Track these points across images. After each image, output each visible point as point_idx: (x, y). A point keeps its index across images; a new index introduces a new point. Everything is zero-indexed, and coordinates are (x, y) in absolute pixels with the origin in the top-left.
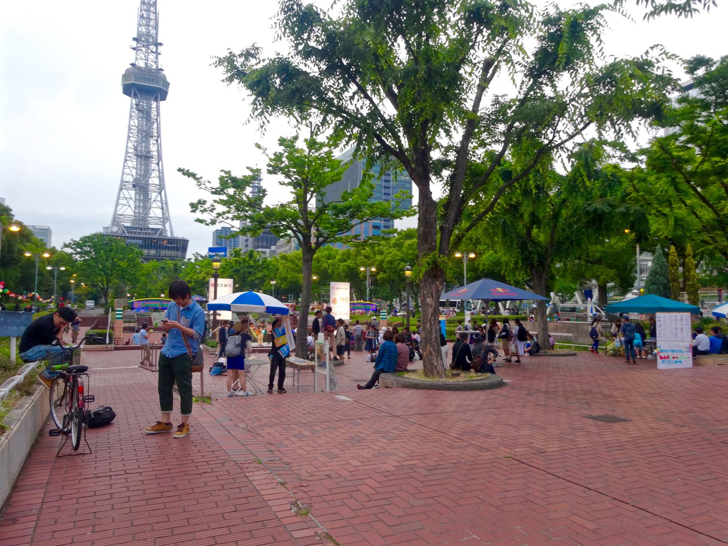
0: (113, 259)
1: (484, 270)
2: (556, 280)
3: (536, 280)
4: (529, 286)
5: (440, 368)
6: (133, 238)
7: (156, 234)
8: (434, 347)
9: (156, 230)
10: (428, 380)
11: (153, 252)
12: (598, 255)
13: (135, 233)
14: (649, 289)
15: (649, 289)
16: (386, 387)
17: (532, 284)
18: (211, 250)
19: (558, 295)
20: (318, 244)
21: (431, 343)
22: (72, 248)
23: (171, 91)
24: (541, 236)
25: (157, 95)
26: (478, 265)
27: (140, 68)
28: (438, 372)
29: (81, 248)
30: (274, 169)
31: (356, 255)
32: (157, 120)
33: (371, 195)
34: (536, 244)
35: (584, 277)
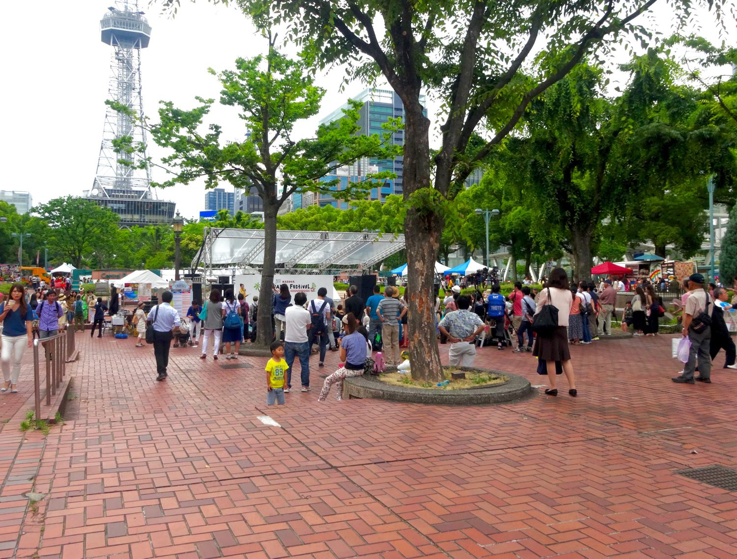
0: (84, 224)
1: (511, 230)
2: (600, 241)
3: (577, 239)
4: (567, 250)
5: (433, 366)
6: (116, 202)
7: (140, 197)
8: (426, 334)
9: (140, 193)
10: (418, 387)
11: (136, 217)
12: (655, 209)
13: (117, 196)
14: (727, 250)
15: (727, 250)
16: (351, 397)
17: (570, 247)
18: (203, 214)
19: (602, 260)
20: (285, 195)
21: (421, 328)
22: (40, 213)
23: (153, 37)
24: (583, 181)
25: (138, 42)
26: (504, 224)
27: (119, 13)
28: (431, 372)
29: (50, 213)
30: (230, 99)
31: (360, 217)
32: (139, 69)
33: (354, 128)
34: (576, 190)
35: (636, 237)
